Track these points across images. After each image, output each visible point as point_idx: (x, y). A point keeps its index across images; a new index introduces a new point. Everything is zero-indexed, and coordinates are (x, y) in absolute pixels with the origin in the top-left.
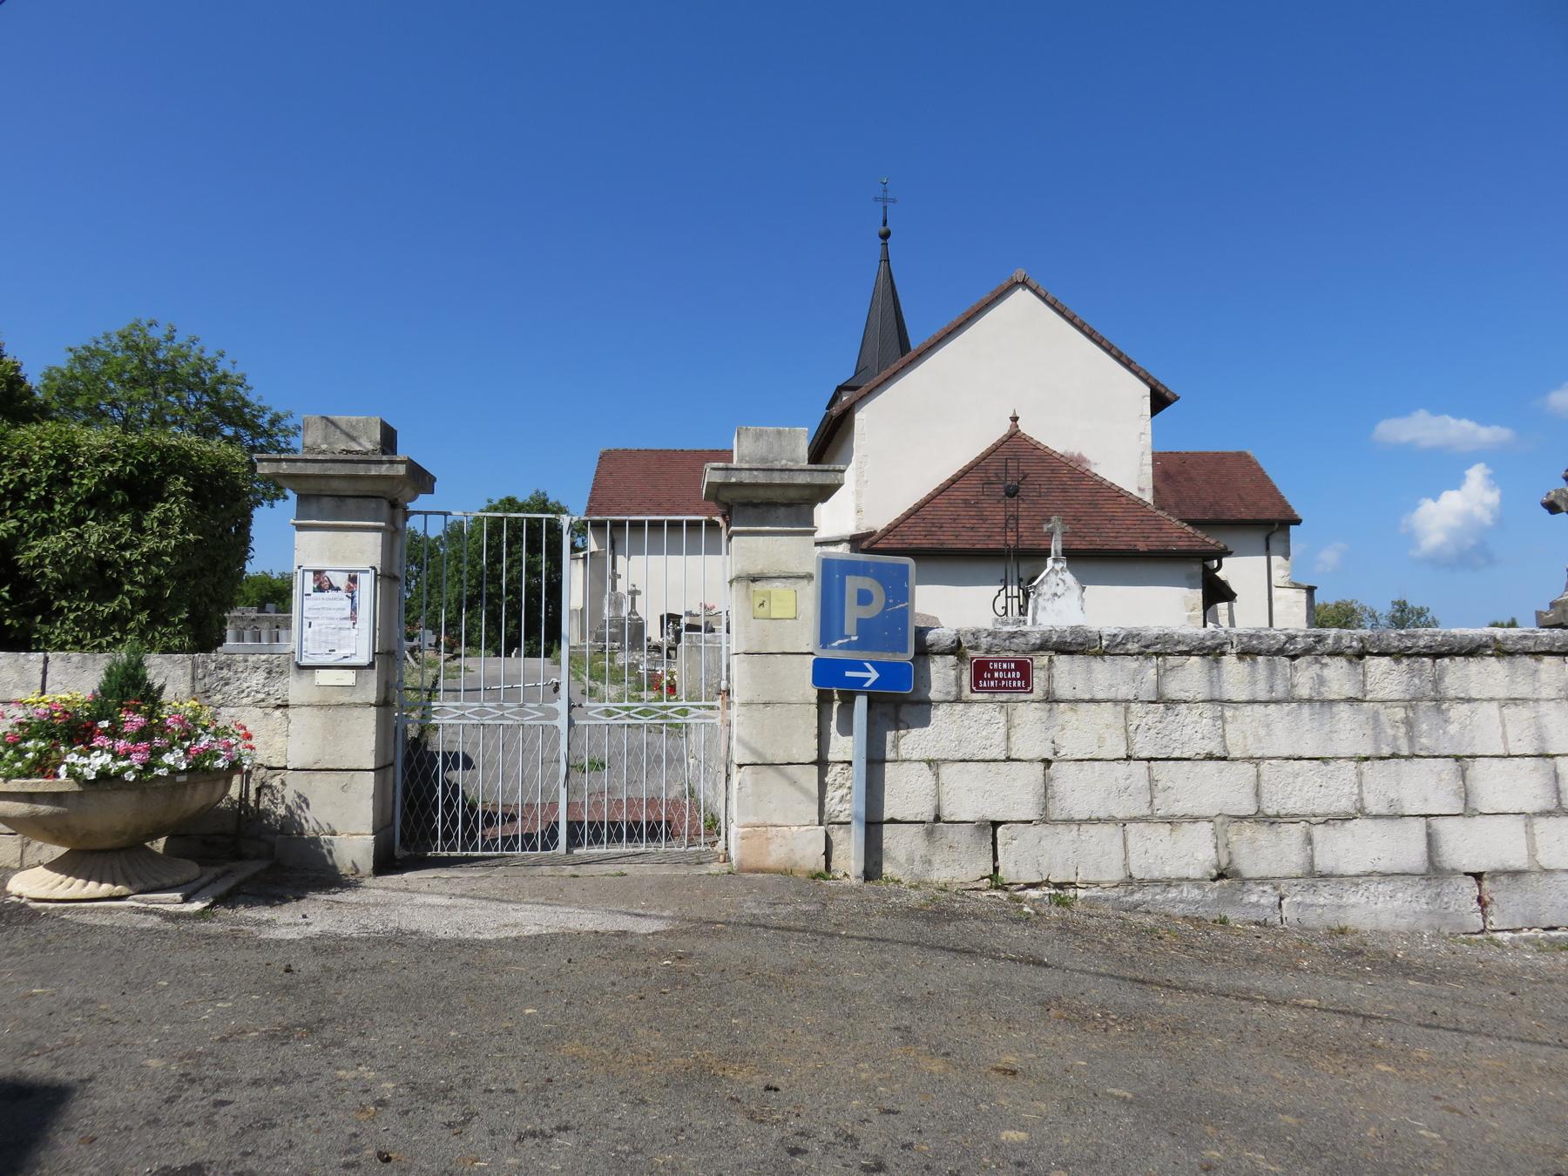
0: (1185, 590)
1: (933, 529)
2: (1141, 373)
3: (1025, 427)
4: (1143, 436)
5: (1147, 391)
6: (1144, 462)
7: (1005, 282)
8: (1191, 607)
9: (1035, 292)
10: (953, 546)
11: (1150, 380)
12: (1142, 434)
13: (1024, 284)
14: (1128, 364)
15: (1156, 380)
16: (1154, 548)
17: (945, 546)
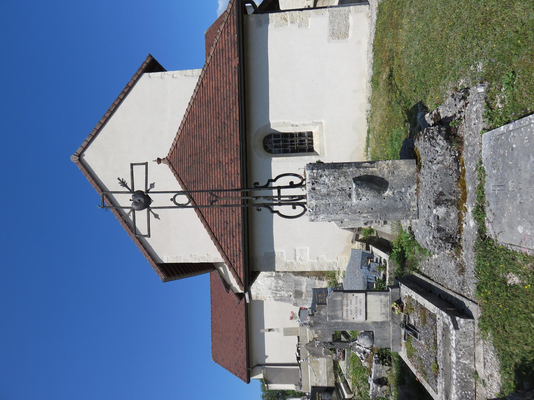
0: (270, 27)
1: (228, 229)
2: (135, 79)
3: (164, 154)
4: (175, 76)
5: (146, 75)
6: (191, 74)
7: (80, 167)
8: (284, 21)
9: (85, 149)
10: (240, 215)
11: (139, 74)
12: (173, 77)
13: (80, 156)
14: (130, 88)
15: (139, 70)
16: (236, 52)
17: (240, 222)
